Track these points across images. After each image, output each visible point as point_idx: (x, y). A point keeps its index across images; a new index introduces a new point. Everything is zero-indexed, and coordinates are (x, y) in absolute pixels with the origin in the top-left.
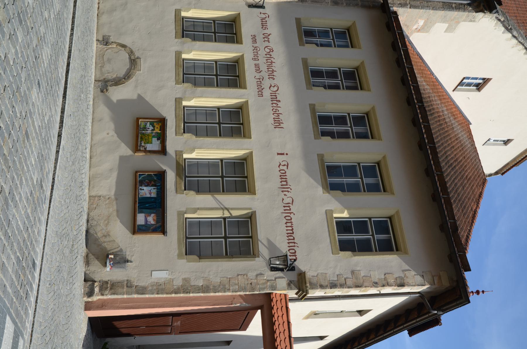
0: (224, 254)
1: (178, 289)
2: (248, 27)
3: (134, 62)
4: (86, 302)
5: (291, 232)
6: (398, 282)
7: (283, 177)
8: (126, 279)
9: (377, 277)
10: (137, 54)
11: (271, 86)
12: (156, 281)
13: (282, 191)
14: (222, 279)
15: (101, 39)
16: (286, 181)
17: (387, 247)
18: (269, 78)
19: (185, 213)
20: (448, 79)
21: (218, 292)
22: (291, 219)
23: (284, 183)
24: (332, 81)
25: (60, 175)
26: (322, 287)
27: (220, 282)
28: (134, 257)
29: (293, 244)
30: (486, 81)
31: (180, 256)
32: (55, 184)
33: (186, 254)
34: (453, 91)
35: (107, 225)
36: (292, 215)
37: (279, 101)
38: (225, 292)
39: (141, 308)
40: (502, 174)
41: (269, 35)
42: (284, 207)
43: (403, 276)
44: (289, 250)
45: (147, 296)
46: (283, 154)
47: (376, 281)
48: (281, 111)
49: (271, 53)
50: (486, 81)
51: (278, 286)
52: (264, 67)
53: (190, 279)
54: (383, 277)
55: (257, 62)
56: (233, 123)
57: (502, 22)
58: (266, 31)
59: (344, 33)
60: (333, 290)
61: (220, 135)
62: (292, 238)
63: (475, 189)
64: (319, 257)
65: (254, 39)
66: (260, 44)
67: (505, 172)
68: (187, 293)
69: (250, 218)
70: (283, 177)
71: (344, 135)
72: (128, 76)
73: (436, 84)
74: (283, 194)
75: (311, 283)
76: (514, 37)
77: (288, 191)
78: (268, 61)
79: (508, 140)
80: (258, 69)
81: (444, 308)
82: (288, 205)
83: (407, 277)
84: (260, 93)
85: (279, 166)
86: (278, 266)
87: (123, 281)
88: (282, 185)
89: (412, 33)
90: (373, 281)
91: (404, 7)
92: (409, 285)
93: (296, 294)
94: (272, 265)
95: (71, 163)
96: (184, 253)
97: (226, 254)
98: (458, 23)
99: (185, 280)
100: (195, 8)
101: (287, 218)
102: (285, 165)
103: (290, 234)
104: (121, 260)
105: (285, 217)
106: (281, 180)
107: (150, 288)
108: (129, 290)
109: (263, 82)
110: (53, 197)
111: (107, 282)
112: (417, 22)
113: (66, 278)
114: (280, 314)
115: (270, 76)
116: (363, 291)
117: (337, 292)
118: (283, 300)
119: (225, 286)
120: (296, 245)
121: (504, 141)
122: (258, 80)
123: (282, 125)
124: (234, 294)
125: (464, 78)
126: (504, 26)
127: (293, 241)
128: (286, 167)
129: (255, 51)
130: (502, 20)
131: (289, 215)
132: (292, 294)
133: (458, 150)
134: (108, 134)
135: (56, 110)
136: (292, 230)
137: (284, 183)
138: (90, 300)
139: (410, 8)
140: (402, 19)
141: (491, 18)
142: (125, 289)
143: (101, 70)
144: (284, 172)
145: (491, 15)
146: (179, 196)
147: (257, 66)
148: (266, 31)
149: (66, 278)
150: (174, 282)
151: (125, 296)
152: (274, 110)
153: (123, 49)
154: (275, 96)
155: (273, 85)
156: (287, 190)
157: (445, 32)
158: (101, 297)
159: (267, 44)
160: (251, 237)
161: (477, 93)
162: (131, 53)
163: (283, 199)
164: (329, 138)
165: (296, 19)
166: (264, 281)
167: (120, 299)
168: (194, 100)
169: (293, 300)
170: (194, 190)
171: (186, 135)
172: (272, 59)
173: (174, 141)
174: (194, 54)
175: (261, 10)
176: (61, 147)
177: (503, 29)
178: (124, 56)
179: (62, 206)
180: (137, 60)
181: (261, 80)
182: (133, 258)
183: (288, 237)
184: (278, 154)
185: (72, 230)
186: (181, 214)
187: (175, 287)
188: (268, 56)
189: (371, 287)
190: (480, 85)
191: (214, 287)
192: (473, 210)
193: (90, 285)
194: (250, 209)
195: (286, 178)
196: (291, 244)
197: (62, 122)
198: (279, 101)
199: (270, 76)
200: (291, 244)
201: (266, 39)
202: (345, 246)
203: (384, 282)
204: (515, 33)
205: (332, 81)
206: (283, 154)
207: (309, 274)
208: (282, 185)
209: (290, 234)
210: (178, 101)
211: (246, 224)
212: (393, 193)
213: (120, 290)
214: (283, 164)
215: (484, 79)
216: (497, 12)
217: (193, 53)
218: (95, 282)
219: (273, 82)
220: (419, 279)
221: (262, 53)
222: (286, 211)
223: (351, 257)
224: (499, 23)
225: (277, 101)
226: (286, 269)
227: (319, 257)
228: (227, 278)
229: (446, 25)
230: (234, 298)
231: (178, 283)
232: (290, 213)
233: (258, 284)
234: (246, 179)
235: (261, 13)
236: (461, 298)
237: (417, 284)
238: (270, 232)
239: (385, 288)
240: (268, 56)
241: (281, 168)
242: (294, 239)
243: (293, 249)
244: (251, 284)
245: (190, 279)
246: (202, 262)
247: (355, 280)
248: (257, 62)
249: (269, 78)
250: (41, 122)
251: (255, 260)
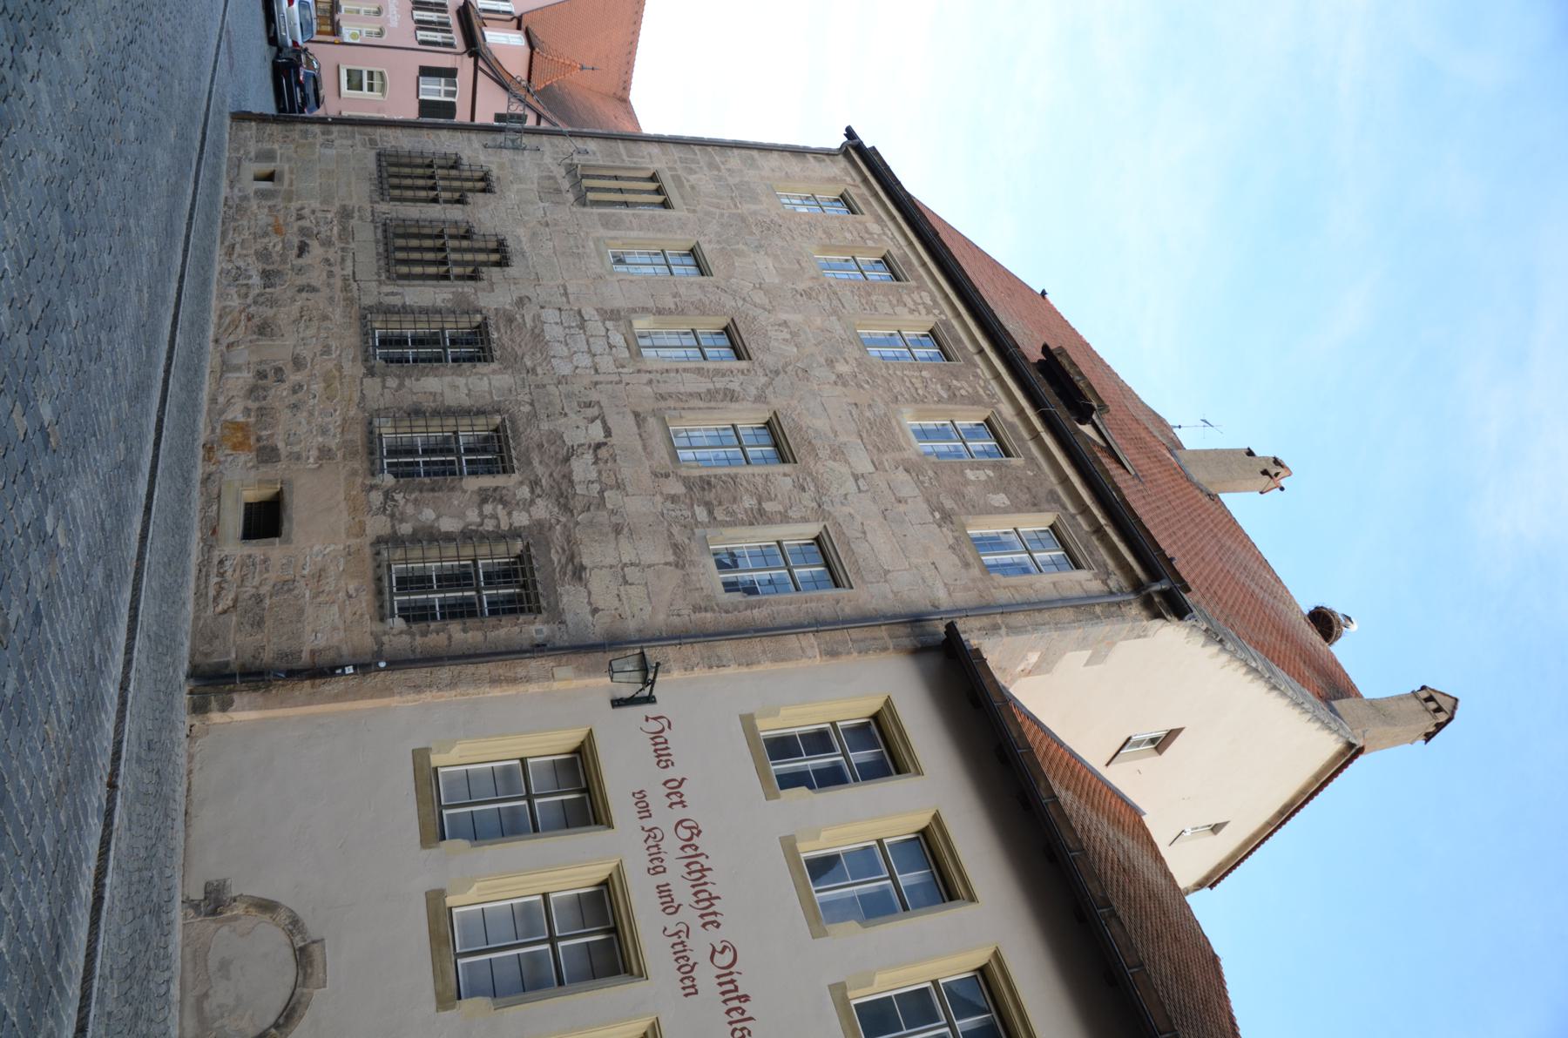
10: (314, 931)
11: (714, 951)
15: (198, 895)
24: (823, 761)
37: (746, 998)
40: (1211, 887)
49: (695, 841)
50: (1172, 734)
52: (683, 892)
61: (536, 830)
66: (664, 817)
67: (1218, 881)
69: (627, 970)
71: (832, 778)
73: (1074, 764)
80: (669, 905)
89: (1013, 681)
98: (1114, 643)
112: (1024, 658)
115: (708, 919)
122: (675, 939)
129: (651, 842)
143: (199, 1008)
145: (1182, 623)
147: (664, 890)
153: (267, 917)
155: (719, 948)
162: (295, 925)
164: (804, 789)
165: (742, 718)
170: (464, 837)
172: (701, 859)
178: (271, 940)
181: (683, 935)
188: (690, 852)
199: (708, 919)
201: (675, 798)
205: (823, 761)
211: (603, 905)
212: (919, 773)
221: (671, 845)
240: (690, 852)
249: (704, 926)
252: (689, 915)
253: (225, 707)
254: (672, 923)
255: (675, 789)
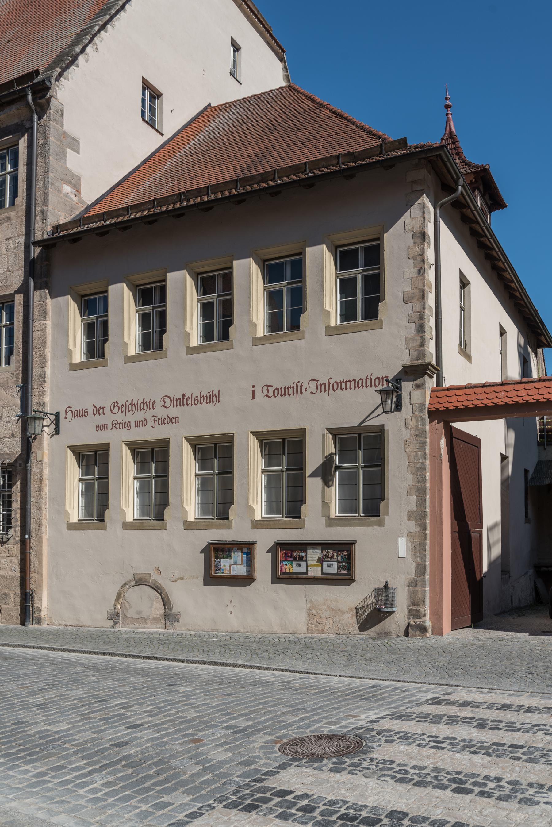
0: (380, 469)
1: (420, 525)
2: (86, 434)
3: (140, 581)
4: (432, 634)
5: (353, 383)
6: (419, 240)
7: (283, 392)
8: (406, 588)
9: (412, 269)
12: (410, 553)
13: (301, 393)
14: (410, 472)
16: (288, 388)
17: (374, 254)
18: (154, 408)
19: (328, 517)
20: (147, 143)
21: (425, 477)
22: (337, 382)
23: (291, 391)
25: (278, 664)
26: (422, 344)
27: (413, 474)
28: (381, 579)
29: (369, 381)
30: (146, 85)
31: (381, 524)
32: (287, 669)
33: (379, 516)
34: (162, 134)
35: (343, 613)
36: (332, 381)
37: (184, 395)
38: (425, 469)
39: (442, 569)
40: (283, 51)
41: (95, 407)
42: (321, 391)
43: (412, 233)
44: (376, 386)
45: (428, 563)
46: (253, 391)
47: (416, 270)
48: (196, 394)
49: (120, 405)
50: (146, 85)
51: (420, 402)
52: (139, 415)
53: (408, 512)
54: (412, 261)
55: (133, 425)
56: (216, 453)
57: (64, 70)
58: (90, 411)
59: (87, 302)
60: (427, 329)
62: (360, 382)
63: (302, 108)
64: (386, 345)
65: (101, 427)
66: (107, 419)
67: (280, 47)
68: (425, 515)
70: (283, 392)
72: (157, 588)
74: (304, 393)
75: (418, 358)
76: (83, 51)
77: (301, 386)
78: (130, 409)
79: (232, 45)
81: (455, 176)
82: (319, 387)
83: (413, 228)
84: (174, 421)
85: (269, 397)
86: (393, 402)
87: (409, 590)
88: (293, 394)
89: (82, 202)
90: (416, 275)
91: (46, 216)
92: (423, 225)
93: (431, 377)
94: (393, 410)
95: (265, 654)
96: (378, 518)
97: (379, 466)
98: (65, 133)
99: (409, 518)
100: (64, 505)
101: (335, 388)
102: (268, 390)
103: (356, 384)
104: (385, 594)
105: (334, 391)
106: (287, 395)
107: (418, 559)
108: (420, 584)
109: (159, 417)
110: (302, 670)
111: (410, 611)
112: (66, 195)
113: (398, 656)
114: (455, 398)
115: (151, 406)
116: (430, 288)
117: (432, 322)
118: (439, 394)
119: (417, 468)
120: (369, 377)
121: (234, 51)
122: (157, 423)
123: (216, 392)
124: (428, 456)
125: (144, 120)
126: (68, 67)
127: (364, 381)
128: (269, 388)
129: (117, 426)
130: (59, 70)
131: (331, 385)
132: (431, 383)
133: (247, 132)
134: (231, 613)
135: (202, 670)
136: (350, 381)
137: (291, 391)
138: (430, 630)
139: (47, 206)
140: (64, 218)
141: (58, 86)
142: (419, 589)
144: (276, 391)
146: (307, 525)
147: (137, 424)
148: (90, 411)
149: (398, 656)
150: (412, 531)
151: (427, 589)
152: (196, 402)
154: (177, 400)
155: (163, 403)
156: (299, 388)
157: (78, 152)
158: (427, 618)
159: (107, 410)
160: (360, 435)
161: (164, 97)
163: (312, 393)
164: (231, 329)
165: (71, 370)
166: (414, 419)
167: (430, 595)
168: (185, 507)
169: (439, 382)
171: (231, 517)
172: (128, 404)
173: (237, 530)
174: (126, 507)
175: (62, 416)
176: (245, 664)
177: (73, 67)
179: (314, 661)
180: (136, 579)
181: (156, 419)
182: (382, 581)
183: (359, 387)
184: (253, 398)
185: (345, 651)
186: (331, 523)
187: (418, 529)
188: (124, 409)
189: (424, 277)
190: (152, 94)
191: (418, 482)
192: (330, 115)
193: (413, 630)
194: (324, 436)
195: (285, 388)
196: (369, 383)
197: (215, 663)
198: (184, 395)
199: (151, 406)
200: (369, 383)
201: (101, 411)
202: (371, 313)
203: (419, 259)
204: (78, 49)
206: (253, 391)
207: (406, 359)
208: (293, 394)
209: (356, 384)
210: (188, 526)
213: (420, 595)
214: (266, 393)
215: (144, 89)
216: (49, 78)
217: (251, 504)
218: (409, 624)
219: (159, 404)
220: (415, 210)
221: (120, 417)
222: (327, 389)
223: (386, 303)
224: (65, 74)
225: (183, 399)
226: (397, 392)
227: (386, 345)
228: (409, 465)
229: (70, 153)
230: (434, 456)
231: (413, 526)
232: (329, 383)
233: (417, 426)
234: (287, 440)
235: (66, 418)
236: (440, 155)
237: (421, 214)
238: (358, 408)
239: (426, 259)
240: (124, 409)
241: (271, 394)
242: (362, 379)
243: (375, 380)
244: (416, 436)
245: (408, 512)
246: (388, 497)
247: (416, 299)
248: (133, 425)
249: (154, 408)
250: (216, 683)
251: (388, 430)
252: (149, 414)
253: (40, 610)
254: (150, 423)
255: (98, 411)
